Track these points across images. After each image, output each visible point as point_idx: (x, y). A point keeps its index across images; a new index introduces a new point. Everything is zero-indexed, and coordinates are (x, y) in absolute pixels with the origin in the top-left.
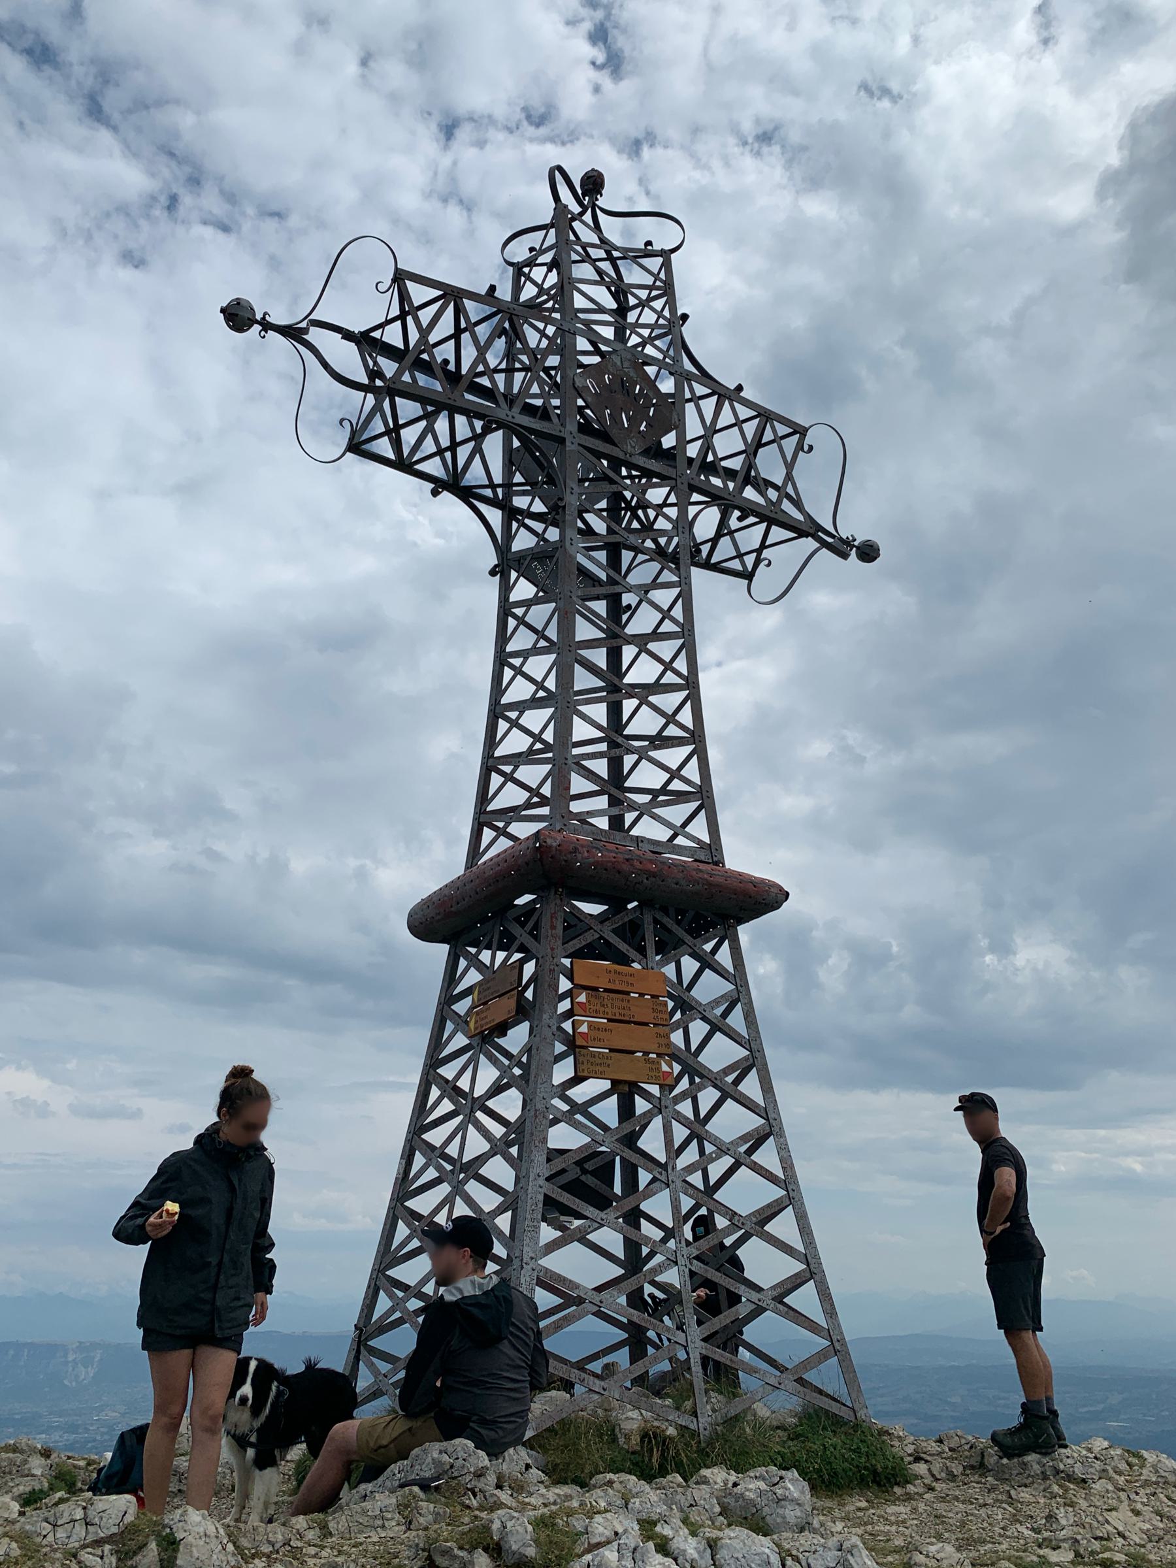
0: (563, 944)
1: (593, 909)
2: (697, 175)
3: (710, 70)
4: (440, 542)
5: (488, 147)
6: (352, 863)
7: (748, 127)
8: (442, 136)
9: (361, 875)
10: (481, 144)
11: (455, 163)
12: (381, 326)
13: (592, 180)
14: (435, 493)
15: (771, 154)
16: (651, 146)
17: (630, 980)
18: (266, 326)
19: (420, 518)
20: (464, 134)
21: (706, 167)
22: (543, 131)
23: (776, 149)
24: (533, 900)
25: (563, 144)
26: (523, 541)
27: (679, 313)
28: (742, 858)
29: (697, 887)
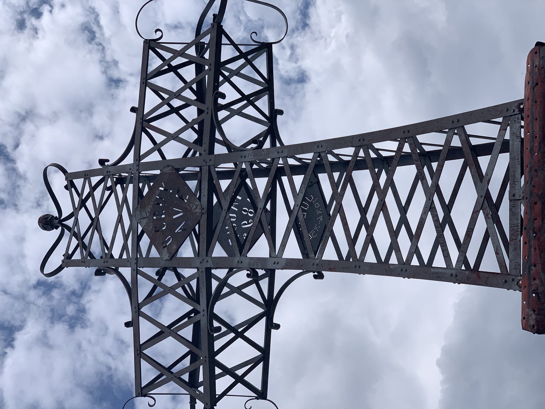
4: (344, 18)
5: (116, 58)
8: (121, 84)
10: (116, 63)
11: (131, 75)
12: (232, 43)
13: (45, 226)
14: (277, 327)
19: (332, 35)
20: (116, 75)
22: (95, 28)
25: (98, 15)
26: (293, 251)
27: (100, 167)
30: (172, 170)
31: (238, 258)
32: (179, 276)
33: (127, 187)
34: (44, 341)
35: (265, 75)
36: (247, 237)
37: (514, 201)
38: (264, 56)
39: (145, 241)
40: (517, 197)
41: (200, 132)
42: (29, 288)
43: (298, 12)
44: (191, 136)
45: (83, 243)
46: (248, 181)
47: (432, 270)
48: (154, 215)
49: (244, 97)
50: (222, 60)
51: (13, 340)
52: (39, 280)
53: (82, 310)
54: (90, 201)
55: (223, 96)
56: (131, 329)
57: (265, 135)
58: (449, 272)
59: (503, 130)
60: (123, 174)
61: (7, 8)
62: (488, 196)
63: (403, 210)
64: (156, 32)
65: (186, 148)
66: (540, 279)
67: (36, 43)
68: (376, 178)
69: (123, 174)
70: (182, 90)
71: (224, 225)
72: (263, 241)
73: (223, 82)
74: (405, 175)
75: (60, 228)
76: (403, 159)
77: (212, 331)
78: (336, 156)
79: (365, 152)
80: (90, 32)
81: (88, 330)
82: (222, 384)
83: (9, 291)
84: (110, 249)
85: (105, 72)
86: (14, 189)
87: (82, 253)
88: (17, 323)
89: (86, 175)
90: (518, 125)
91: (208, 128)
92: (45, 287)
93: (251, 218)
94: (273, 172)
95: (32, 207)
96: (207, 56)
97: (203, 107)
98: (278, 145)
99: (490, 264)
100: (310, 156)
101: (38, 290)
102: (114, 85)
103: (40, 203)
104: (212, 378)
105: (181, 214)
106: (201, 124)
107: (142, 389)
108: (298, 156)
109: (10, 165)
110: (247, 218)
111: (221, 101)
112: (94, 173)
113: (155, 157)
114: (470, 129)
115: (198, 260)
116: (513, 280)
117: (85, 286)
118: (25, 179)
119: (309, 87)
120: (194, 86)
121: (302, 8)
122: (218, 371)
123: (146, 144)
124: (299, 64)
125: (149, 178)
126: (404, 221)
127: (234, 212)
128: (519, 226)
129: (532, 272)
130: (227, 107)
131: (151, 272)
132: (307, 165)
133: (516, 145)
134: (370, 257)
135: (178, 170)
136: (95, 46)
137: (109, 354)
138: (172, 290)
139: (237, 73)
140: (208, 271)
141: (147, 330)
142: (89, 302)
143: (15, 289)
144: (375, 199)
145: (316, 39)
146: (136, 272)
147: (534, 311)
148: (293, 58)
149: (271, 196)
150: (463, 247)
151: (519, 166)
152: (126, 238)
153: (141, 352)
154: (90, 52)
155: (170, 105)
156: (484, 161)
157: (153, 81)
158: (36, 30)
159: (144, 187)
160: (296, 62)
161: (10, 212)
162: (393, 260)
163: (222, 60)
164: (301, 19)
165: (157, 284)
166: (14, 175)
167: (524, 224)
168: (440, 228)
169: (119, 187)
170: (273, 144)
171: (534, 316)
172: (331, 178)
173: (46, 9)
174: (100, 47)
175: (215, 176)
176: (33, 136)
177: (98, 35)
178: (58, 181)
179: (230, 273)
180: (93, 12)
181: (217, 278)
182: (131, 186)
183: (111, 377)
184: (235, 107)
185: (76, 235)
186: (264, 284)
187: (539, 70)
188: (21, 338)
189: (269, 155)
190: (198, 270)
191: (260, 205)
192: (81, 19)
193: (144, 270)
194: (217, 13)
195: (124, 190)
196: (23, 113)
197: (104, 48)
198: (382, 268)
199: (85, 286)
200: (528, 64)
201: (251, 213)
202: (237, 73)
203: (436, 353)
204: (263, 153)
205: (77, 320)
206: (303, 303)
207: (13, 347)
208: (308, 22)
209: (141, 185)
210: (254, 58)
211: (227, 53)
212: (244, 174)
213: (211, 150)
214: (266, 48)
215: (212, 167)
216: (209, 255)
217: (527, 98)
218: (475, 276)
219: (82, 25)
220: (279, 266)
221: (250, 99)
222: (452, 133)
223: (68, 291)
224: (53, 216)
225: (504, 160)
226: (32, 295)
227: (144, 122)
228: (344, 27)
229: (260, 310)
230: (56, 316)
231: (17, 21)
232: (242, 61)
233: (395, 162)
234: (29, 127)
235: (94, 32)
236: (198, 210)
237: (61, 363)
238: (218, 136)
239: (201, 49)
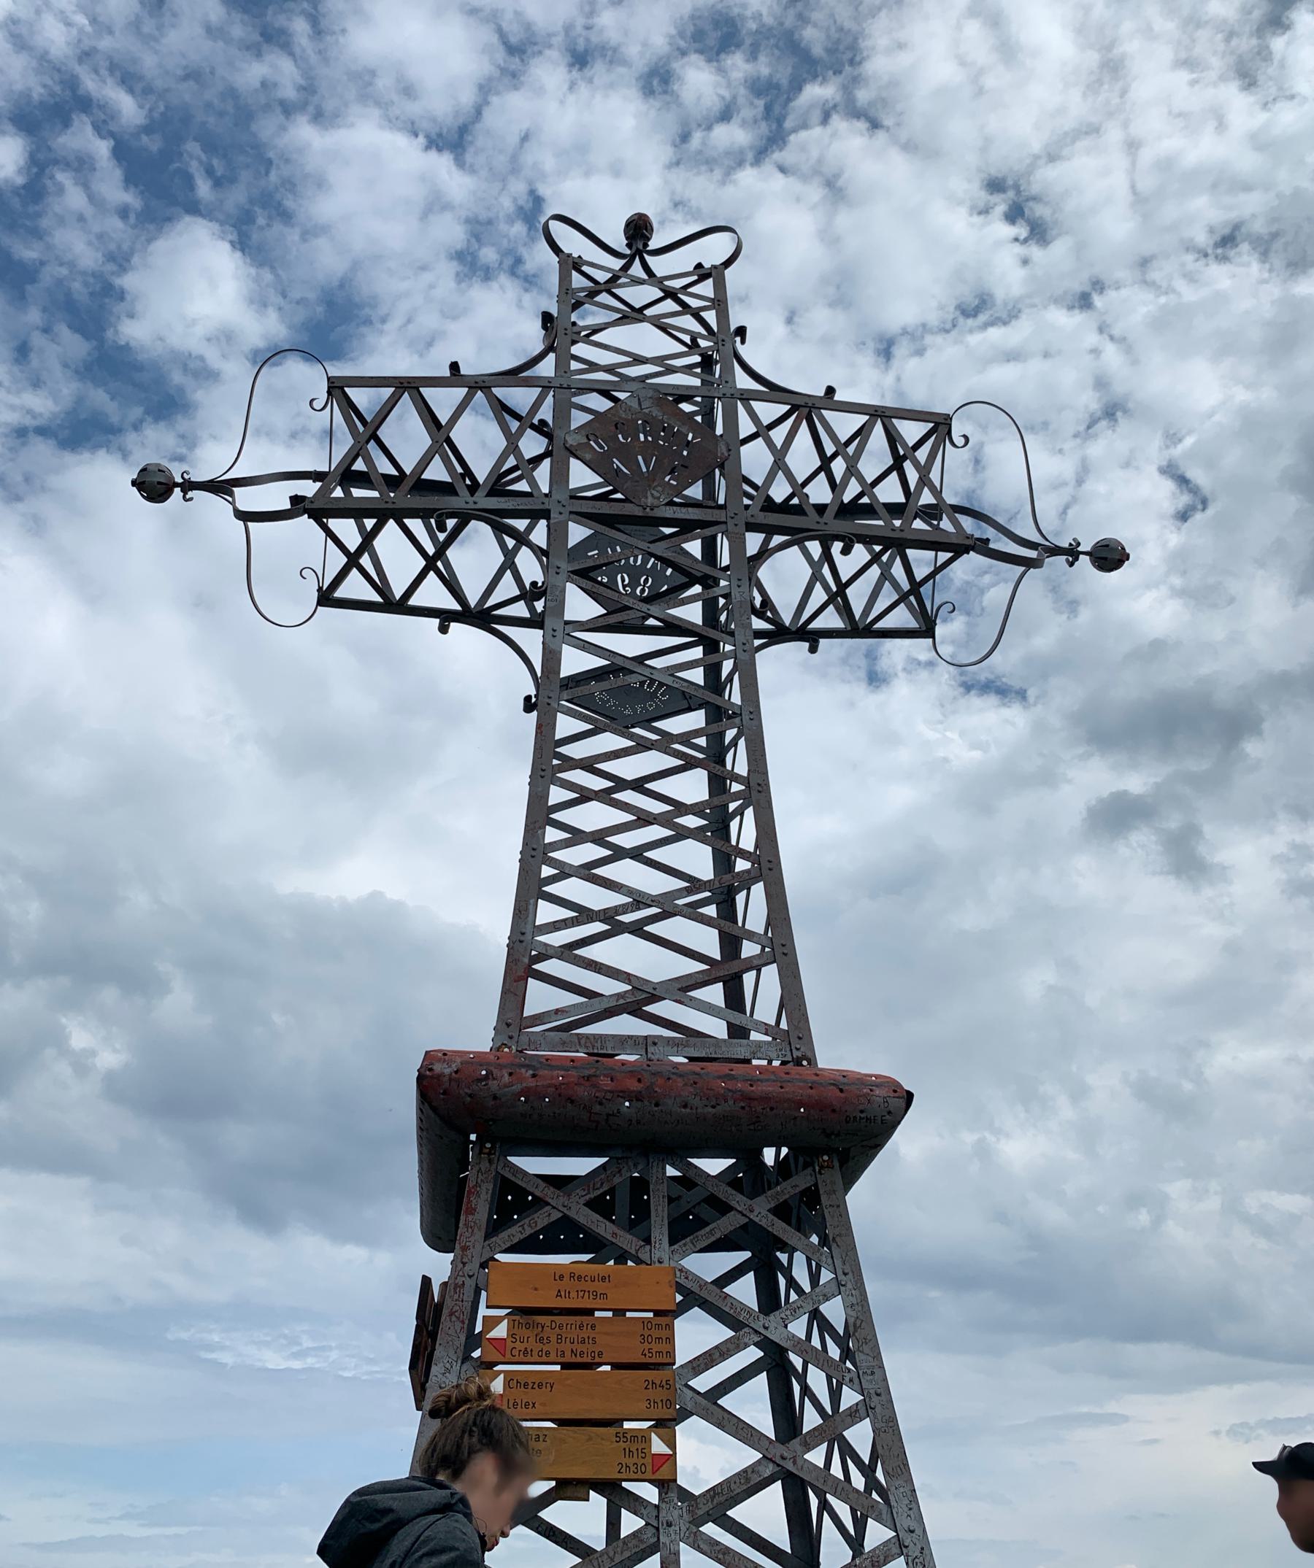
0: (487, 1237)
1: (714, 1166)
2: (1163, 300)
3: (1139, 200)
4: (977, 754)
5: (929, 353)
6: (970, 1138)
7: (1202, 238)
8: (882, 359)
9: (983, 1152)
11: (898, 379)
12: (938, 570)
14: (443, 629)
15: (1240, 254)
16: (1101, 293)
17: (600, 1287)
18: (188, 486)
19: (948, 734)
20: (900, 351)
21: (1169, 290)
22: (982, 318)
23: (1245, 247)
24: (603, 1166)
25: (1005, 323)
26: (574, 662)
27: (733, 328)
28: (840, 1050)
29: (723, 1108)
30: (717, 457)
31: (565, 566)
32: (537, 460)
33: (695, 375)
34: (435, 204)
35: (879, 625)
36: (601, 583)
37: (645, 1043)
38: (913, 624)
39: (600, 403)
40: (651, 1049)
41: (785, 507)
42: (530, 183)
43: (991, 677)
44: (779, 492)
45: (598, 293)
46: (697, 589)
47: (532, 901)
48: (645, 422)
49: (842, 587)
50: (909, 551)
51: (440, 150)
52: (543, 200)
53: (487, 275)
54: (674, 307)
55: (846, 551)
56: (448, 374)
57: (776, 621)
58: (529, 929)
59: (766, 1029)
60: (718, 366)
61: (1028, 161)
62: (654, 998)
63: (637, 854)
64: (966, 437)
65: (759, 482)
66: (510, 1085)
67: (963, 211)
68: (696, 810)
69: (718, 366)
70: (861, 479)
71: (623, 545)
72: (590, 610)
73: (871, 551)
74: (696, 859)
75: (628, 252)
76: (723, 859)
77: (440, 516)
78: (734, 743)
79: (738, 793)
80: (977, 308)
81: (453, 284)
82: (347, 530)
83: (526, 145)
84: (587, 340)
85: (905, 332)
86: (707, 162)
87: (583, 289)
88: (469, 157)
89: (719, 303)
90: (773, 1055)
91: (789, 521)
92: (531, 209)
93: (634, 590)
94: (712, 634)
95: (673, 193)
96: (918, 524)
97: (830, 513)
98: (757, 642)
99: (539, 998)
100: (736, 698)
101: (525, 197)
102: (882, 347)
103: (680, 207)
104: (356, 512)
105: (644, 470)
106: (799, 510)
107: (342, 388)
108: (736, 677)
109: (750, 156)
110: (634, 583)
111: (837, 547)
112: (723, 316)
113: (746, 427)
114: (771, 973)
115: (563, 497)
116: (511, 1037)
117: (530, 283)
118: (723, 183)
119: (859, 690)
120: (865, 500)
121: (999, 684)
122: (369, 523)
123: (768, 411)
124: (901, 674)
125: (708, 414)
126: (619, 854)
127: (645, 562)
128: (602, 1050)
129: (523, 1070)
130: (827, 556)
131: (546, 413)
132: (721, 694)
133: (740, 1051)
134: (557, 795)
135: (722, 467)
136: (951, 317)
137: (409, 321)
138: (513, 446)
139: (886, 576)
140: (545, 514)
141: (443, 401)
142: (502, 288)
143: (528, 159)
144: (657, 807)
145: (942, 706)
146: (545, 386)
147: (456, 1072)
148: (913, 665)
149: (672, 627)
150: (567, 952)
151: (703, 1055)
152: (610, 369)
153: (405, 389)
154: (941, 307)
155: (834, 456)
156: (714, 995)
157: (879, 429)
158: (985, 211)
159: (695, 404)
160: (904, 669)
161: (667, 153)
162: (552, 835)
163: (909, 551)
164: (979, 682)
165: (526, 421)
166: (732, 163)
167: (605, 1060)
168: (606, 915)
169: (697, 359)
170: (759, 634)
171: (447, 1071)
172: (697, 733)
173: (1021, 230)
174: (948, 326)
175: (708, 532)
176: (798, 200)
177: (970, 322)
178: (713, 250)
179: (539, 552)
180: (1010, 315)
181: (530, 529)
182: (697, 382)
183: (368, 322)
184: (826, 570)
185: (615, 278)
186: (520, 610)
187: (865, 1095)
188: (442, 164)
189: (746, 623)
190: (546, 495)
191: (654, 609)
192: (999, 294)
193: (549, 400)
194: (991, 546)
195: (688, 369)
196: (840, 183)
197: (947, 331)
198: (539, 814)
199: (531, 282)
200: (876, 1076)
201: (643, 591)
202: (886, 576)
203: (395, 891)
204: (745, 617)
205: (469, 265)
206: (487, 671)
207: (428, 148)
208: (973, 692)
209: (699, 399)
210: (910, 607)
211: (922, 561)
212: (710, 582)
213: (752, 527)
214: (926, 630)
215: (723, 527)
216: (573, 516)
217: (819, 1073)
218: (521, 973)
219: (991, 296)
220: (549, 637)
221: (838, 597)
222: (765, 942)
223: (523, 252)
224: (649, 239)
225: (716, 1028)
226: (518, 187)
227: (806, 411)
228: (962, 755)
229: (473, 600)
230: (479, 228)
231: (1004, 179)
232: (905, 586)
233: (719, 844)
234: (815, 193)
235: (975, 316)
236: (650, 501)
237: (395, 234)
238: (777, 539)
239: (931, 513)
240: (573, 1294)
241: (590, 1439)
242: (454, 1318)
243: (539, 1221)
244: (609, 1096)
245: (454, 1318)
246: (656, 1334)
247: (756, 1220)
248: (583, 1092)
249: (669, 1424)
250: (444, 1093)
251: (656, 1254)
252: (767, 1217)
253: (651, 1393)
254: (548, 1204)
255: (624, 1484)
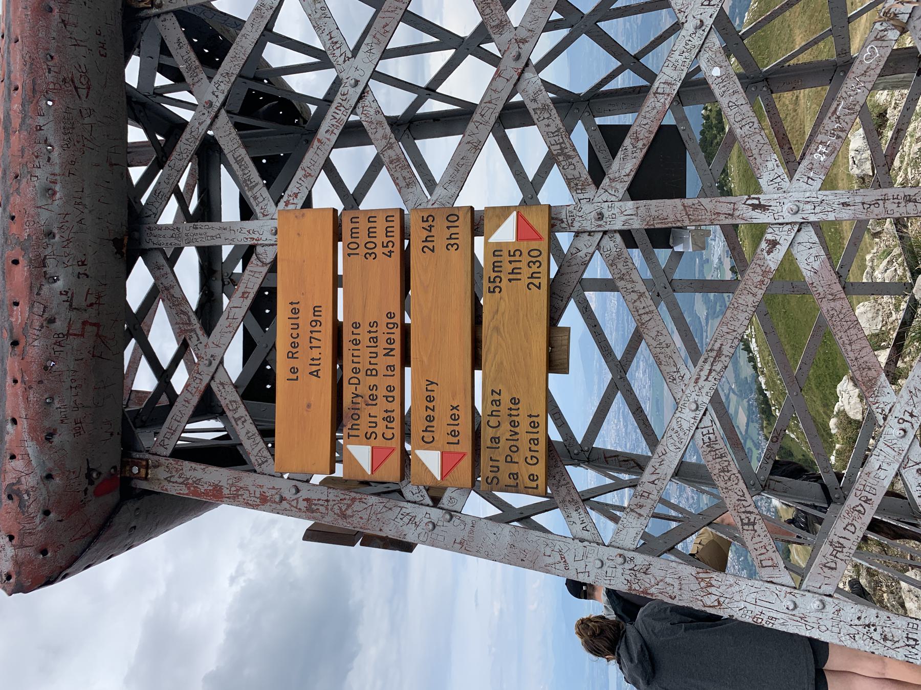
17: (306, 316)
209: (238, 269)
240: (315, 353)
241: (497, 329)
242: (349, 512)
243: (229, 398)
244: (38, 309)
245: (349, 512)
246: (363, 238)
247: (222, 98)
248: (35, 348)
249: (476, 217)
250: (44, 552)
251: (267, 237)
252: (218, 84)
253: (440, 241)
254: (208, 388)
255: (552, 276)
